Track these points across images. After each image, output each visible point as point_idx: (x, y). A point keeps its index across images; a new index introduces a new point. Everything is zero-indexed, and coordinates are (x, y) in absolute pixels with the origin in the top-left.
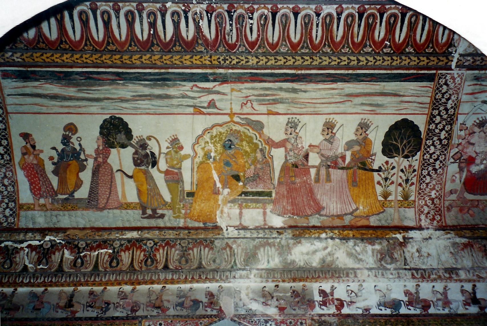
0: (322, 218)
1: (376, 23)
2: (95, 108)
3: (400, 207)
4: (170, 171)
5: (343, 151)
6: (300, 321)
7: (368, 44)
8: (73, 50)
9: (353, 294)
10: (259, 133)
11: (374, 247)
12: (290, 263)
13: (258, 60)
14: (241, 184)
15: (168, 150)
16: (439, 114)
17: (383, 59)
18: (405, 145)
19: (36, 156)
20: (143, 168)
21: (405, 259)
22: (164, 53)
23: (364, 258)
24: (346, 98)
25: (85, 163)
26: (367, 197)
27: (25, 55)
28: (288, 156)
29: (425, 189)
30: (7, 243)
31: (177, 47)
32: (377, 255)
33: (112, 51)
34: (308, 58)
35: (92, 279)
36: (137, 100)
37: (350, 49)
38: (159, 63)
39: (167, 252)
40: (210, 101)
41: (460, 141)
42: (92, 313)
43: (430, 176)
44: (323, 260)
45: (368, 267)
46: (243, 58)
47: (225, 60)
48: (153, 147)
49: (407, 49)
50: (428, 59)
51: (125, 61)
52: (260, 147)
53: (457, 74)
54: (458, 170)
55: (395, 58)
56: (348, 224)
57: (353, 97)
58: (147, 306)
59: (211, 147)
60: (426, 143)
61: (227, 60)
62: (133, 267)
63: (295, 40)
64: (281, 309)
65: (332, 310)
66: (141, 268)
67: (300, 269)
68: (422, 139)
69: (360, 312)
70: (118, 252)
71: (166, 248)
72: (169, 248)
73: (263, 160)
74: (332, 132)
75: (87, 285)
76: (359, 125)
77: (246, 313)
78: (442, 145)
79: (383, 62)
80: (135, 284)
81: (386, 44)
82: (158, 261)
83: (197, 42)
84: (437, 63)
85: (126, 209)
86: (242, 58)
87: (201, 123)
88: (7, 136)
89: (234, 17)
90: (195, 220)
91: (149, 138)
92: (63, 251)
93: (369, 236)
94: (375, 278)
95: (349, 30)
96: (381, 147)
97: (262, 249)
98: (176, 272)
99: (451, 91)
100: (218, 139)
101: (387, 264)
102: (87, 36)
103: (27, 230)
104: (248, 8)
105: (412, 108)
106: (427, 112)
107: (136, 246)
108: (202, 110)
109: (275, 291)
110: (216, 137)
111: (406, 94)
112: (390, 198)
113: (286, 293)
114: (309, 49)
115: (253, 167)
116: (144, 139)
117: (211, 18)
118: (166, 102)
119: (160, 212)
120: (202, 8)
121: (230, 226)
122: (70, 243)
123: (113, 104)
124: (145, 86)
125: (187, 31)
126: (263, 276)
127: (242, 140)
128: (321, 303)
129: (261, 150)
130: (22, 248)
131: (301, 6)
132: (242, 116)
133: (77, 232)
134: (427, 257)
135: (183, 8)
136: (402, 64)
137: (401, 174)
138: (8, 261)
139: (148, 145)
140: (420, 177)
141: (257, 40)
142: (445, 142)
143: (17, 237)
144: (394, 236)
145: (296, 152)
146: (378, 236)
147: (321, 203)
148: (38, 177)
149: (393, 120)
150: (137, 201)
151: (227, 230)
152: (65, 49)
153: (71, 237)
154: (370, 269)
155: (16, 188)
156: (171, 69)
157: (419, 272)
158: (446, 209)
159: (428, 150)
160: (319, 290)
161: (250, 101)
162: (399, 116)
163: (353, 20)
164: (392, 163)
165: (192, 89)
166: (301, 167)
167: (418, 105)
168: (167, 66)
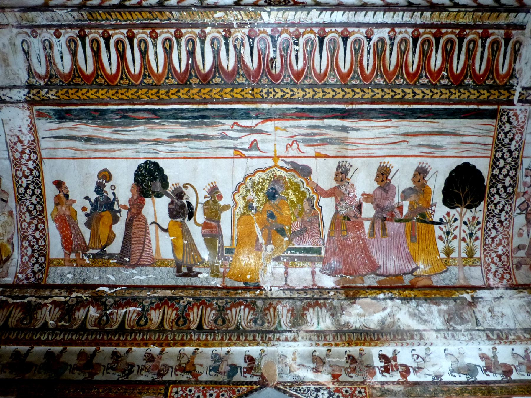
1: (432, 50)
2: (129, 151)
6: (358, 389)
7: (424, 74)
8: (108, 85)
10: (306, 180)
11: (439, 307)
12: (344, 325)
14: (287, 239)
16: (502, 157)
19: (69, 207)
20: (179, 220)
21: (477, 319)
22: (203, 86)
23: (429, 319)
24: (401, 138)
25: (118, 214)
26: (428, 254)
29: (491, 245)
32: (444, 316)
33: (149, 84)
36: (174, 142)
37: (405, 80)
38: (197, 98)
40: (252, 142)
41: (526, 189)
42: (114, 376)
43: (496, 229)
44: (383, 322)
46: (288, 91)
47: (268, 93)
48: (190, 197)
49: (465, 81)
50: (488, 92)
51: (161, 96)
52: (308, 196)
54: (525, 222)
55: (453, 91)
56: (409, 284)
57: (410, 137)
58: (176, 370)
59: (252, 196)
61: (271, 93)
62: (163, 326)
63: (345, 70)
64: (335, 377)
65: (396, 377)
66: (172, 327)
67: (356, 331)
68: (485, 187)
69: (430, 379)
70: (147, 310)
71: (201, 307)
73: (311, 211)
74: (387, 178)
75: (111, 345)
77: (293, 380)
78: (507, 193)
79: (440, 96)
83: (239, 73)
84: (498, 97)
85: (160, 266)
90: (235, 280)
91: (185, 186)
94: (444, 340)
95: (402, 57)
96: (441, 196)
97: (311, 310)
98: (210, 333)
101: (457, 325)
102: (123, 68)
104: (293, 32)
105: (474, 150)
106: (489, 155)
107: (168, 304)
108: (243, 152)
109: (328, 356)
110: (258, 184)
111: (466, 133)
112: (453, 255)
113: (340, 358)
114: (360, 80)
115: (299, 219)
116: (180, 187)
117: (253, 44)
120: (243, 33)
123: (149, 147)
124: (183, 124)
125: (228, 60)
129: (309, 200)
130: (46, 305)
133: (106, 289)
134: (502, 317)
135: (224, 33)
136: (462, 97)
137: (464, 227)
141: (303, 70)
142: (509, 190)
144: (461, 296)
146: (442, 295)
147: (377, 261)
148: (70, 230)
149: (454, 163)
150: (171, 257)
151: (271, 290)
152: (101, 84)
153: (99, 293)
154: (438, 331)
155: (47, 241)
156: (211, 104)
157: (495, 332)
158: (514, 266)
159: (493, 199)
161: (296, 141)
162: (459, 159)
165: (232, 127)
166: (354, 219)
167: (479, 146)
168: (206, 101)
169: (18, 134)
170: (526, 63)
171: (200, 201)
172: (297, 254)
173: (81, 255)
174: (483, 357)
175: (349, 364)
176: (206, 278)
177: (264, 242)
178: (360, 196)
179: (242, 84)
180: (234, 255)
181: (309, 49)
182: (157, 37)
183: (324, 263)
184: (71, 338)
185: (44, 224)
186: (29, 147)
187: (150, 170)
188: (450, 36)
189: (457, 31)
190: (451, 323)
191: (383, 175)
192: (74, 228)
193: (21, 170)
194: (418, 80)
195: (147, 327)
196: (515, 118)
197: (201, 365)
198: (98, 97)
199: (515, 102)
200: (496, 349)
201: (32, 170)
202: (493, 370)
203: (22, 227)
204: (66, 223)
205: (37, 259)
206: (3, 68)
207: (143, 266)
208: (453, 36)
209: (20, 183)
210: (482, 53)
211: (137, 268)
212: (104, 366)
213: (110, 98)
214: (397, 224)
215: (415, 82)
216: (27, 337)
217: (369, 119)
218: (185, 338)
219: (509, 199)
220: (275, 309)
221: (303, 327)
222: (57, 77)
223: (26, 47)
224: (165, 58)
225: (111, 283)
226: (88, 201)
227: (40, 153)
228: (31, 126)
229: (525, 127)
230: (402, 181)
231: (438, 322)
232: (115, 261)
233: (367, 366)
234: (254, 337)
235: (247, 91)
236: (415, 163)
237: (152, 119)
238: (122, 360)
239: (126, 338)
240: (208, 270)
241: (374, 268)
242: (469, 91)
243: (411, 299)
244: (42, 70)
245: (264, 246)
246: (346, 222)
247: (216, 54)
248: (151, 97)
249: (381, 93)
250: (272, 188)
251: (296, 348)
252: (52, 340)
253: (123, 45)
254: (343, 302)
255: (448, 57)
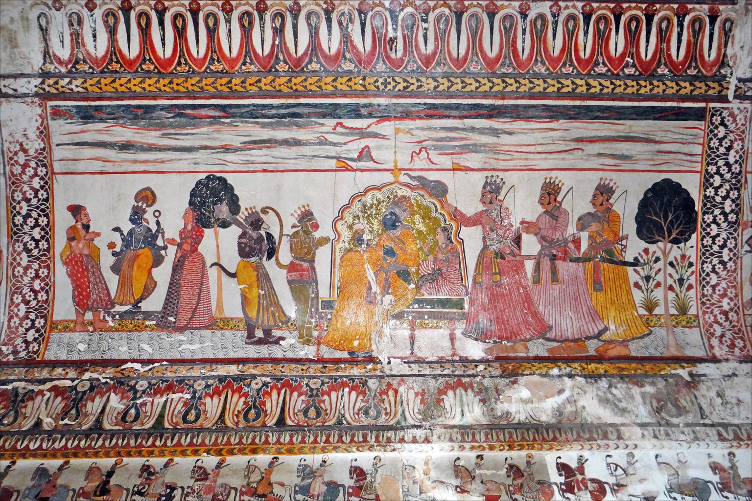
0: (549, 343)
1: (610, 30)
2: (185, 161)
3: (674, 326)
4: (298, 265)
5: (575, 231)
7: (601, 61)
8: (159, 72)
9: (620, 471)
10: (440, 201)
11: (643, 390)
12: (501, 417)
13: (436, 84)
14: (412, 286)
15: (295, 230)
17: (625, 84)
18: (671, 222)
20: (252, 260)
21: (701, 408)
22: (295, 74)
23: (629, 407)
24: (573, 145)
25: (163, 252)
26: (621, 309)
27: (89, 82)
28: (487, 240)
29: (711, 296)
30: (16, 384)
31: (314, 65)
32: (651, 403)
33: (218, 72)
34: (512, 81)
35: (150, 443)
38: (285, 90)
39: (285, 398)
40: (363, 149)
44: (559, 412)
45: (639, 421)
46: (414, 81)
47: (386, 83)
48: (271, 224)
49: (659, 70)
50: (691, 84)
52: (443, 225)
53: (739, 109)
55: (642, 83)
56: (595, 354)
57: (585, 143)
58: (242, 494)
60: (703, 219)
61: (390, 83)
62: (223, 422)
63: (492, 55)
66: (237, 424)
67: (520, 426)
68: (697, 213)
70: (200, 398)
71: (283, 391)
72: (288, 392)
73: (447, 245)
74: (555, 200)
75: (140, 454)
76: (597, 189)
78: (729, 223)
79: (625, 89)
80: (223, 452)
81: (628, 62)
82: (268, 412)
83: (344, 57)
84: (706, 91)
86: (411, 81)
87: (348, 184)
88: (48, 211)
89: (400, 18)
90: (335, 348)
91: (265, 210)
92: (109, 397)
93: (633, 372)
94: (654, 441)
97: (450, 393)
99: (731, 135)
100: (374, 212)
101: (672, 416)
102: (181, 50)
103: (54, 364)
106: (699, 169)
109: (478, 466)
110: (371, 207)
112: (657, 311)
113: (497, 470)
115: (431, 258)
117: (365, 20)
118: (294, 151)
119: (276, 333)
120: (352, 6)
121: (395, 358)
122: (122, 383)
123: (214, 156)
124: (264, 125)
125: (330, 40)
126: (454, 439)
127: (413, 213)
128: (563, 487)
129: (445, 229)
131: (499, 3)
132: (413, 174)
133: (137, 366)
134: (738, 405)
135: (325, 6)
137: (670, 270)
138: (12, 413)
139: (263, 222)
140: (701, 275)
141: (434, 54)
142: (732, 217)
143: (37, 375)
144: (673, 372)
145: (501, 232)
147: (546, 319)
148: (87, 277)
150: (241, 315)
151: (389, 363)
152: (148, 72)
153: (126, 373)
154: (643, 425)
156: (305, 97)
157: (730, 429)
159: (708, 230)
160: (557, 464)
161: (425, 148)
163: (576, 26)
164: (655, 252)
165: (335, 129)
166: (510, 257)
167: (684, 157)
168: (297, 94)
169: (20, 140)
170: (742, 47)
171: (285, 231)
172: (428, 309)
173: (102, 313)
174: (715, 468)
175: (511, 479)
176: (292, 346)
177: (378, 291)
178: (518, 225)
179: (350, 72)
180: (334, 312)
181: (441, 26)
182: (232, 10)
183: (468, 322)
184: (78, 445)
185: (49, 269)
186: (36, 157)
187: (214, 188)
188: (634, 12)
189: (644, 6)
190: (663, 414)
191: (550, 194)
192: (93, 273)
193: (21, 191)
194: (593, 69)
195: (198, 424)
196: (731, 119)
197: (282, 485)
198: (144, 89)
199: (730, 98)
200: (734, 455)
201: (38, 190)
202: (733, 489)
203: (13, 275)
204: (82, 266)
205: (33, 321)
206: (8, 50)
207: (195, 329)
208: (639, 13)
209: (18, 209)
210: (680, 35)
211: (187, 332)
212: (128, 490)
213: (160, 90)
214: (572, 266)
215: (589, 71)
216: (7, 444)
217: (528, 119)
218: (257, 441)
219: (732, 230)
220: (396, 392)
221: (440, 420)
222: (85, 62)
223: (43, 23)
224: (242, 38)
225: (146, 357)
226: (118, 234)
227: (52, 166)
228: (42, 128)
229: (747, 132)
230: (577, 203)
231: (643, 413)
232: (154, 322)
233: (539, 483)
234: (365, 437)
235: (357, 80)
236: (594, 179)
237: (220, 117)
238: (157, 478)
239: (165, 442)
240: (295, 333)
241: (543, 331)
242: (664, 84)
243: (600, 376)
244: (64, 53)
245: (379, 297)
246: (500, 260)
247: (314, 33)
248: (220, 88)
249: (543, 85)
250: (391, 213)
251: (430, 454)
252: (47, 450)
253: (184, 20)
254: (498, 380)
255: (632, 38)
